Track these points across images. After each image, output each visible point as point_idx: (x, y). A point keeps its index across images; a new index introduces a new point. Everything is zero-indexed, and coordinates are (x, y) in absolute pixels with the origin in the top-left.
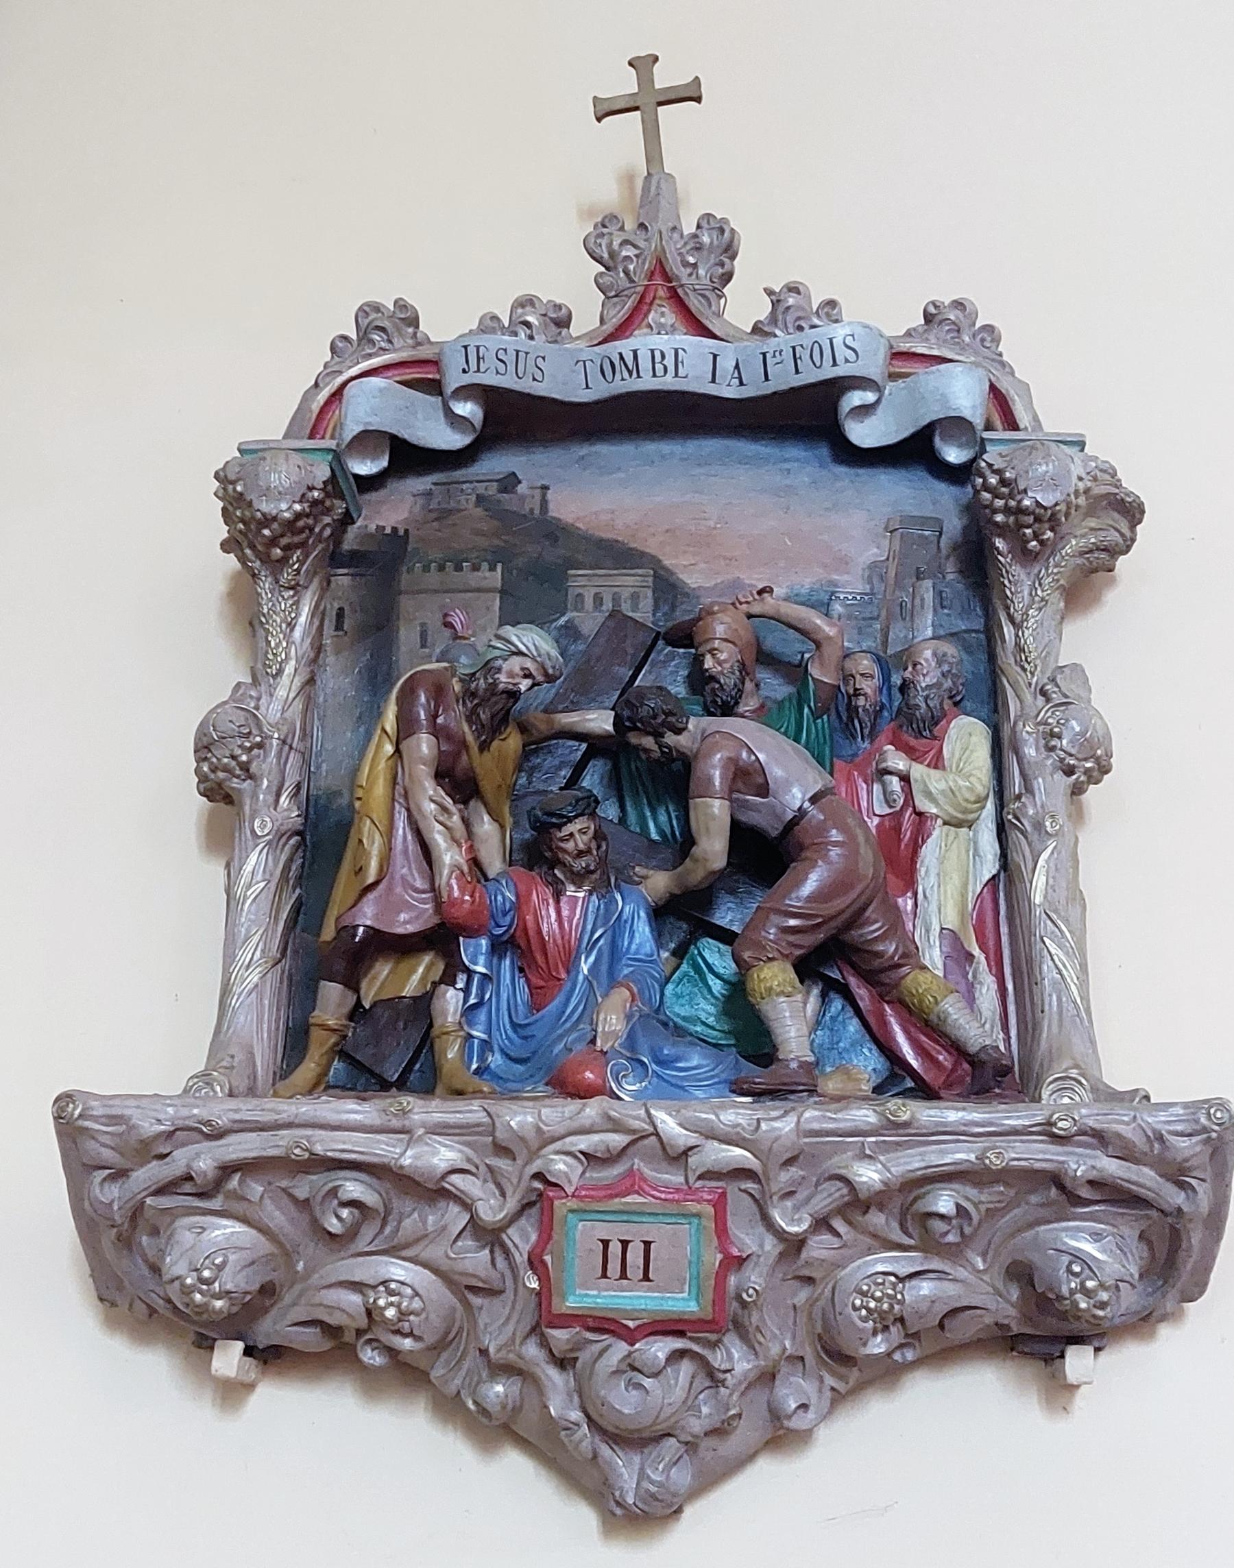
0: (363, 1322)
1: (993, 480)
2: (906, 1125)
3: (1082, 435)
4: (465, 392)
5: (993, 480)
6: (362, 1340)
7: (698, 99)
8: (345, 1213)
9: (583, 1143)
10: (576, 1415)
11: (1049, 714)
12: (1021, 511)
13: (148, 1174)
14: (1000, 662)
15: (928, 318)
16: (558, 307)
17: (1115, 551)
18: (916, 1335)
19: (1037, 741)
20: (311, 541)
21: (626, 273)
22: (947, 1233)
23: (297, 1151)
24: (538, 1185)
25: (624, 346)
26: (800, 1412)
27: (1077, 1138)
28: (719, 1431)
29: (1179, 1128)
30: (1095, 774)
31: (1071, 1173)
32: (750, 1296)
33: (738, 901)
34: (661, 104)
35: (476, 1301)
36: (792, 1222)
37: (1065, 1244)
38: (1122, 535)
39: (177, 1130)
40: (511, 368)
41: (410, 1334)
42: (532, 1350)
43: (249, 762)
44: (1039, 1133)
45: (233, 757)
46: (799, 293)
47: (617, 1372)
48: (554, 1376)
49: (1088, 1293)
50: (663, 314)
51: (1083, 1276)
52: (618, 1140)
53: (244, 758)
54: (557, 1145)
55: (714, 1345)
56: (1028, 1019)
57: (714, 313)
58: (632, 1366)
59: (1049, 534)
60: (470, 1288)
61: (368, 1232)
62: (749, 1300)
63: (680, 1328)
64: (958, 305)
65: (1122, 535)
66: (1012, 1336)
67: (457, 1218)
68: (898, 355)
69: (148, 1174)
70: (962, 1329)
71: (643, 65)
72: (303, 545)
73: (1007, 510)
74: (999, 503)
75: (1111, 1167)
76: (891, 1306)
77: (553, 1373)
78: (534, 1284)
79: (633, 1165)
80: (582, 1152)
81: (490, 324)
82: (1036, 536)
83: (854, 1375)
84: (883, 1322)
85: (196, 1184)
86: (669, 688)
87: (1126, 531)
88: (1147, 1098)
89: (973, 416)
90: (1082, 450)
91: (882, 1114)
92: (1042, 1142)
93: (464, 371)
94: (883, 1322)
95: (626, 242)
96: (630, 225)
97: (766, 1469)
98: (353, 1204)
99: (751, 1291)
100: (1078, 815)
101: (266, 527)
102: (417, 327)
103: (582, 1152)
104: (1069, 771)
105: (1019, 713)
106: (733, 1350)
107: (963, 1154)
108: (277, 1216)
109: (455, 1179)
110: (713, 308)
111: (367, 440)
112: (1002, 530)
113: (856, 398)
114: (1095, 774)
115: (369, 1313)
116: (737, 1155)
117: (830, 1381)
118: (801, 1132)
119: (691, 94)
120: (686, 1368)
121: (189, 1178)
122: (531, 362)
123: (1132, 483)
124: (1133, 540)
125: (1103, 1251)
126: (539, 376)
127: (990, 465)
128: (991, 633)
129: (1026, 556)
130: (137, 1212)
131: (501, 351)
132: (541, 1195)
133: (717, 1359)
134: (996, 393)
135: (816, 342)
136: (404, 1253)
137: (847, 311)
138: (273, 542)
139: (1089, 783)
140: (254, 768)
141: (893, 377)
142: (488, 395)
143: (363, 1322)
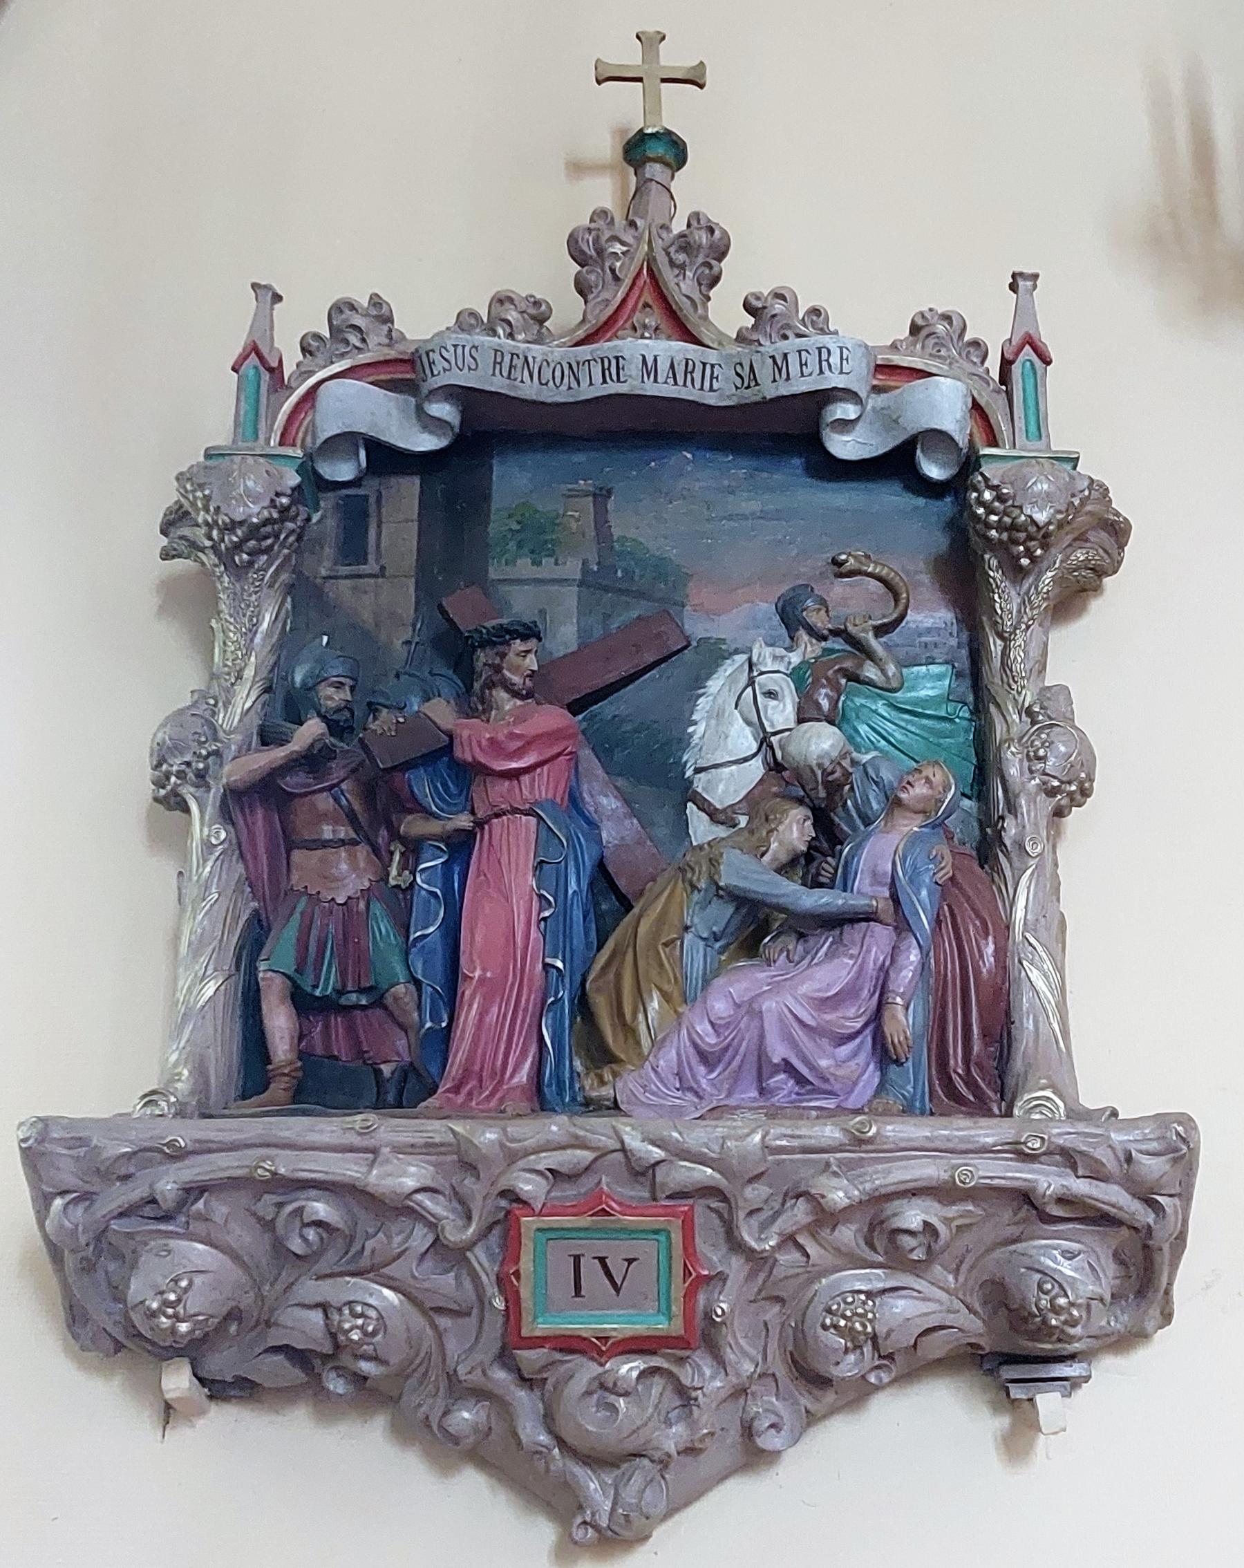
0: (327, 1348)
1: (987, 495)
2: (870, 1141)
7: (701, 86)
8: (311, 1234)
10: (543, 1438)
12: (1014, 527)
14: (986, 681)
15: (915, 329)
16: (537, 303)
17: (1100, 572)
18: (890, 1357)
19: (1021, 761)
20: (276, 547)
21: (613, 271)
22: (912, 1250)
23: (260, 1171)
24: (504, 1203)
25: (605, 347)
26: (773, 1431)
28: (690, 1451)
30: (1078, 797)
34: (664, 80)
35: (444, 1322)
36: (759, 1240)
37: (1039, 1262)
39: (140, 1150)
40: (453, 362)
41: (375, 1358)
42: (500, 1375)
43: (206, 768)
46: (785, 299)
47: (589, 1393)
48: (521, 1397)
49: (1056, 1310)
51: (1053, 1293)
52: (586, 1156)
53: (201, 766)
54: (521, 1164)
55: (681, 1361)
57: (700, 317)
58: (604, 1386)
59: (1039, 552)
60: (439, 1310)
61: (331, 1256)
64: (947, 318)
66: (982, 1356)
67: (420, 1239)
68: (880, 368)
70: (937, 1346)
71: (650, 41)
72: (270, 549)
73: (1000, 527)
74: (994, 518)
75: (1081, 1187)
76: (865, 1326)
77: (522, 1394)
79: (600, 1182)
81: (466, 321)
82: (1029, 553)
83: (830, 1397)
85: (160, 1207)
86: (519, 703)
88: (1114, 1113)
89: (894, 437)
90: (1075, 468)
91: (845, 1130)
92: (1011, 1159)
95: (615, 238)
96: (620, 221)
97: (733, 1486)
98: (319, 1224)
100: (1055, 835)
102: (392, 323)
103: (549, 1170)
104: (1052, 793)
105: (1005, 737)
106: (705, 1368)
107: (929, 1170)
108: (243, 1236)
109: (419, 1197)
110: (700, 311)
111: (345, 442)
113: (848, 411)
114: (1078, 797)
115: (333, 1336)
117: (805, 1401)
118: (766, 1147)
120: (658, 1384)
123: (1121, 503)
124: (1120, 563)
125: (1076, 1270)
126: (473, 367)
127: (986, 479)
128: (977, 653)
129: (1017, 573)
130: (101, 1235)
132: (508, 1213)
133: (686, 1376)
138: (238, 547)
141: (877, 390)
142: (463, 396)
143: (327, 1348)
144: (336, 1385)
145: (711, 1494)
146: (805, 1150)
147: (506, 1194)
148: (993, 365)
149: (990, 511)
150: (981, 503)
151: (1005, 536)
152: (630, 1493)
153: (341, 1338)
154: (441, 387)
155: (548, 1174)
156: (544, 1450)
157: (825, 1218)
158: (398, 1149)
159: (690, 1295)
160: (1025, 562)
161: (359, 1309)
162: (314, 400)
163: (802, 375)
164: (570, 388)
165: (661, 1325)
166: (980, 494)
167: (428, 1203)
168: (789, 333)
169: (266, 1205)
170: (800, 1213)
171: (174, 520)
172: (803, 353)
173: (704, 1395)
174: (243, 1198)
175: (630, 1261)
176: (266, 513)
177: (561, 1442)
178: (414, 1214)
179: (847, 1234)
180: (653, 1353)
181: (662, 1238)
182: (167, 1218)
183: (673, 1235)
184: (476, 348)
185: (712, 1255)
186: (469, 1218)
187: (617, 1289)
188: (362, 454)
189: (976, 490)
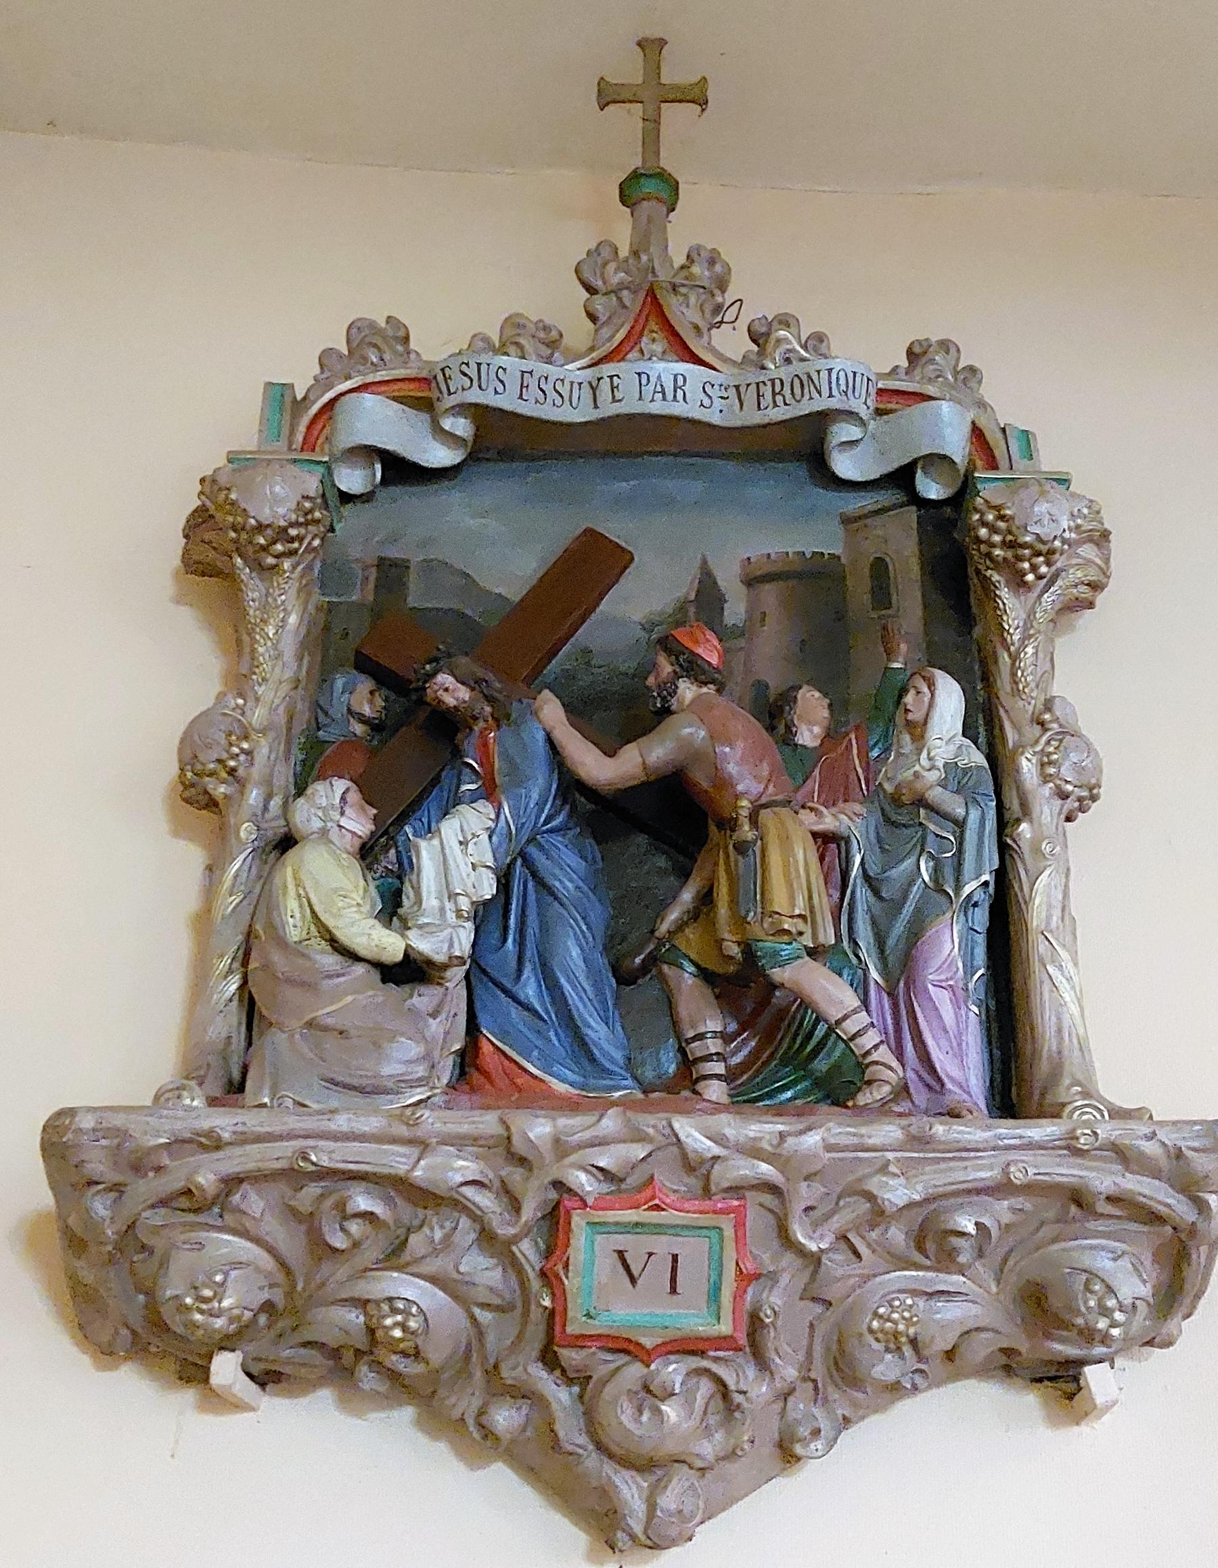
0: (362, 1342)
4: (464, 409)
5: (990, 517)
8: (355, 1227)
10: (583, 1439)
13: (146, 1188)
16: (546, 329)
27: (1093, 1152)
29: (1196, 1144)
31: (499, 1412)
44: (1061, 1148)
45: (219, 761)
50: (654, 343)
53: (232, 763)
54: (572, 1158)
63: (701, 1346)
69: (146, 1188)
74: (997, 538)
75: (1133, 1184)
78: (547, 1302)
82: (1034, 568)
84: (893, 1342)
88: (1151, 1117)
94: (893, 1342)
104: (1064, 796)
107: (985, 1172)
109: (465, 1190)
112: (997, 565)
115: (371, 1331)
116: (765, 1169)
119: (697, 96)
121: (188, 1192)
126: (559, 384)
131: (500, 370)
134: (977, 433)
135: (797, 376)
136: (415, 1270)
137: (835, 347)
140: (241, 772)
141: (879, 412)
142: (480, 414)
143: (362, 1342)
144: (368, 1378)
147: (558, 1185)
149: (993, 530)
150: (984, 524)
152: (669, 1500)
153: (380, 1334)
154: (471, 404)
155: (594, 1170)
156: (580, 1451)
157: (879, 1215)
159: (739, 1296)
160: (1030, 577)
161: (400, 1305)
164: (811, 398)
166: (982, 514)
170: (854, 1211)
171: (199, 521)
172: (761, 385)
174: (282, 1188)
175: (650, 1254)
176: (294, 517)
177: (600, 1447)
178: (456, 1204)
179: (897, 1235)
180: (702, 1353)
183: (726, 1233)
184: (504, 370)
185: (765, 1255)
187: (633, 1280)
188: (378, 467)
189: (976, 510)
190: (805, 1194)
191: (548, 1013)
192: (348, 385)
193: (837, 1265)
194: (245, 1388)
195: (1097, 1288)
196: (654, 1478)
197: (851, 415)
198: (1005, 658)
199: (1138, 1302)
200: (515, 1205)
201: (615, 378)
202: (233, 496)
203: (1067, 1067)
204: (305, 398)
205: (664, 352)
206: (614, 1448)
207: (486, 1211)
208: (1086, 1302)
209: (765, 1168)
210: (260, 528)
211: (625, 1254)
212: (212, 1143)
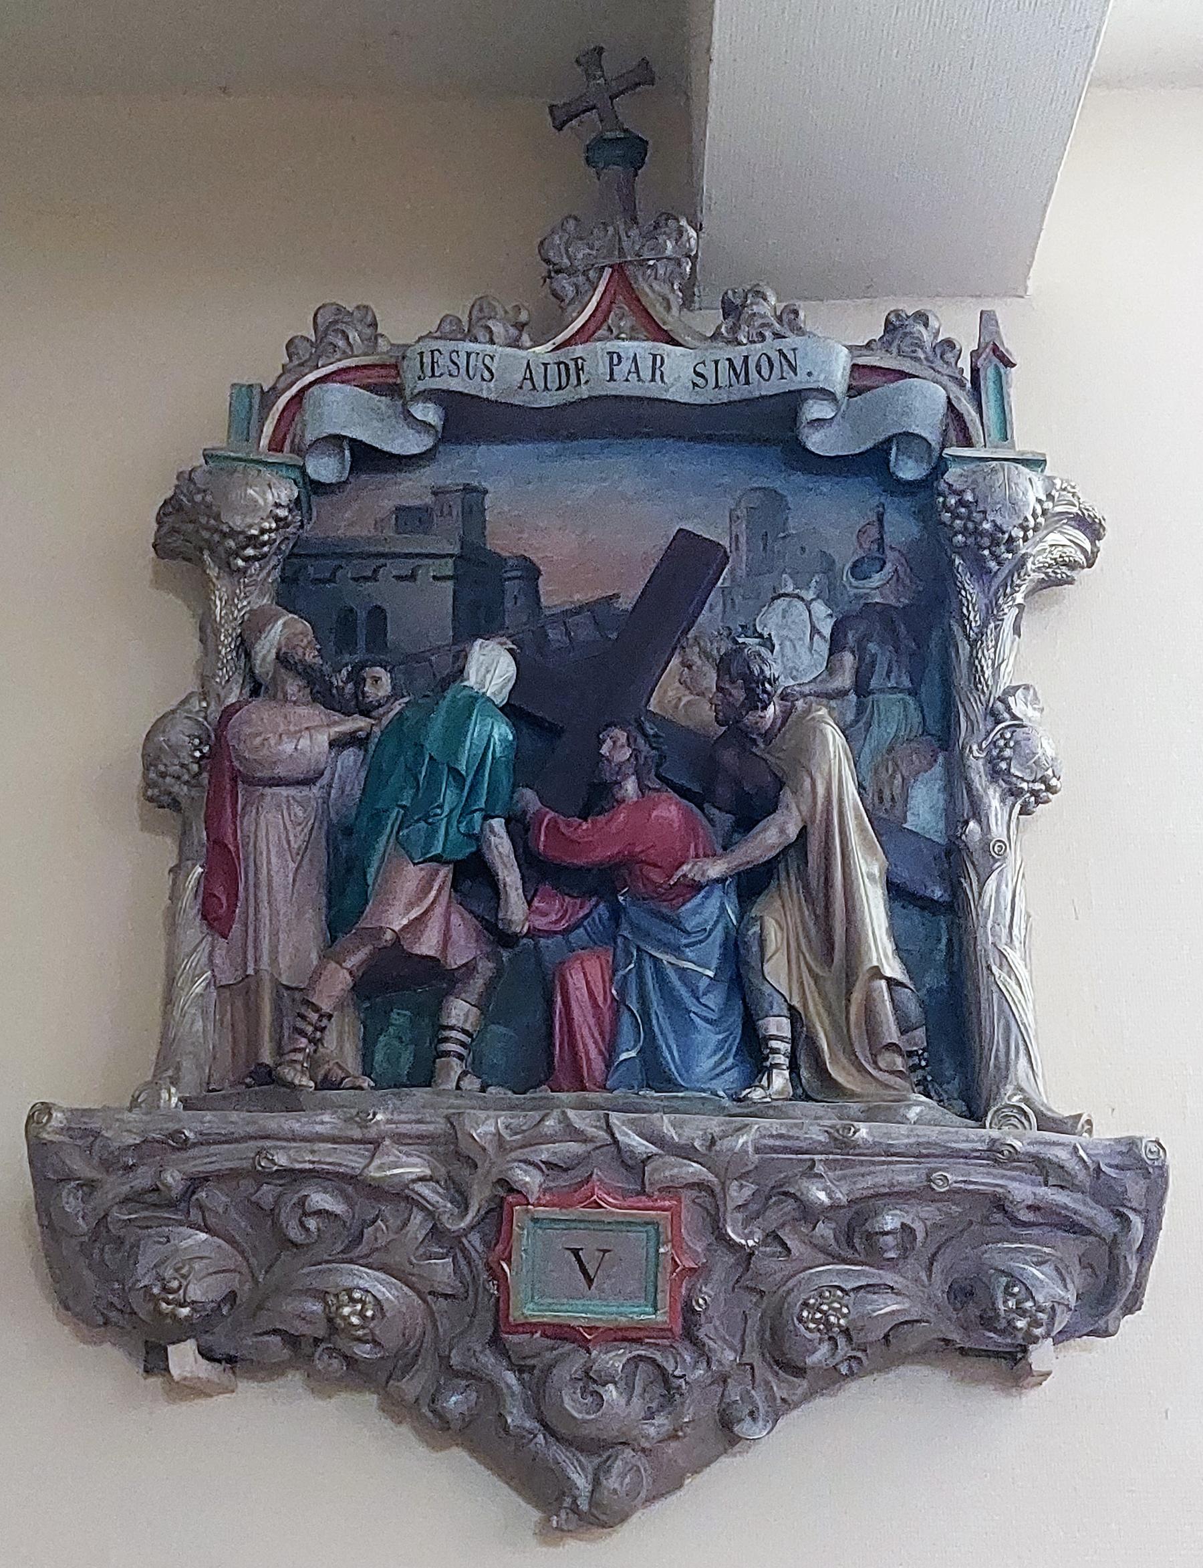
3: (1044, 455)
6: (320, 1350)
9: (544, 1153)
11: (998, 736)
15: (889, 327)
32: (700, 1306)
33: (168, 1388)
38: (1083, 550)
40: (463, 370)
42: (488, 1359)
56: (837, 938)
62: (698, 1309)
65: (1083, 550)
67: (418, 1224)
72: (264, 556)
80: (543, 1162)
83: (803, 1384)
87: (1087, 545)
93: (419, 378)
98: (319, 1213)
99: (701, 1301)
101: (237, 555)
103: (543, 1162)
109: (419, 1187)
112: (961, 550)
115: (330, 1320)
122: (480, 359)
129: (981, 571)
139: (1037, 803)
145: (715, 1466)
146: (786, 1150)
147: (503, 1183)
148: (965, 363)
151: (971, 541)
155: (543, 1166)
157: (808, 1213)
158: (400, 1139)
161: (357, 1295)
162: (301, 402)
163: (612, 379)
165: (646, 1316)
166: (945, 497)
167: (426, 1192)
168: (767, 334)
169: (267, 1193)
172: (436, 353)
173: (687, 1383)
181: (652, 1233)
182: (172, 1205)
186: (467, 1209)
187: (590, 1281)
189: (940, 495)
190: (738, 1193)
191: (1017, 1048)
192: (310, 378)
193: (770, 1265)
194: (204, 1370)
195: (1016, 1290)
196: (597, 1461)
197: (826, 394)
198: (964, 648)
199: (1059, 1309)
200: (463, 1205)
201: (436, 352)
202: (209, 498)
203: (1011, 1076)
204: (273, 388)
205: (633, 328)
206: (562, 1430)
207: (437, 1206)
208: (1005, 1302)
209: (694, 1168)
210: (233, 534)
211: (581, 1253)
212: (177, 1143)
